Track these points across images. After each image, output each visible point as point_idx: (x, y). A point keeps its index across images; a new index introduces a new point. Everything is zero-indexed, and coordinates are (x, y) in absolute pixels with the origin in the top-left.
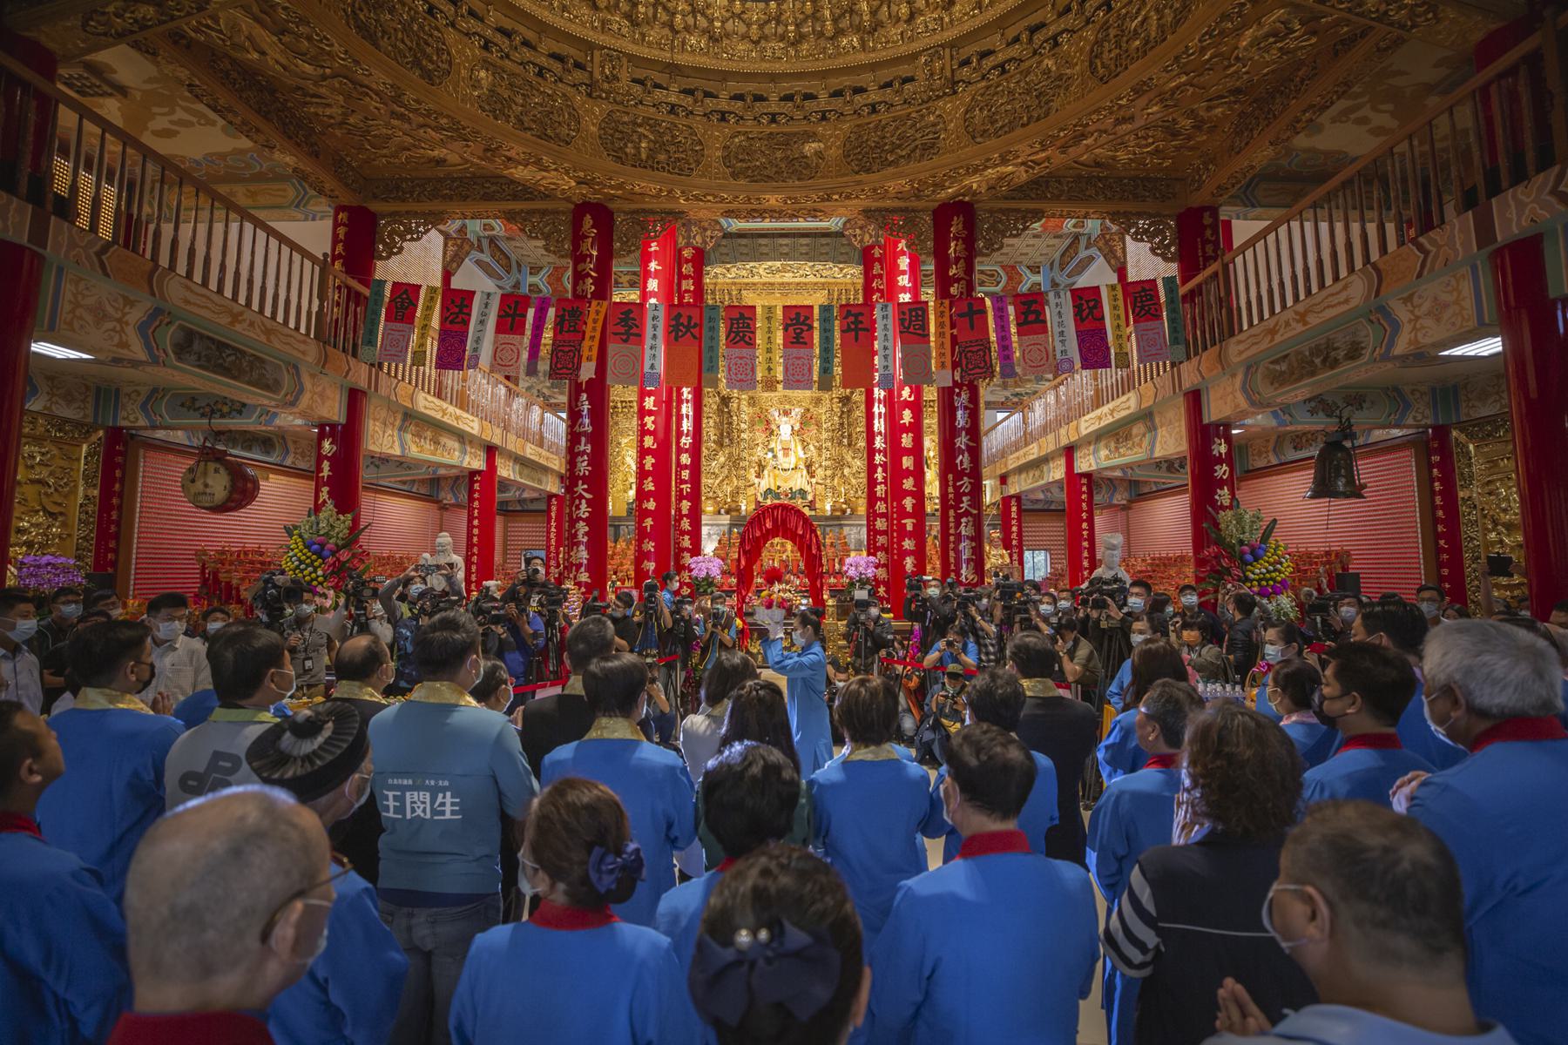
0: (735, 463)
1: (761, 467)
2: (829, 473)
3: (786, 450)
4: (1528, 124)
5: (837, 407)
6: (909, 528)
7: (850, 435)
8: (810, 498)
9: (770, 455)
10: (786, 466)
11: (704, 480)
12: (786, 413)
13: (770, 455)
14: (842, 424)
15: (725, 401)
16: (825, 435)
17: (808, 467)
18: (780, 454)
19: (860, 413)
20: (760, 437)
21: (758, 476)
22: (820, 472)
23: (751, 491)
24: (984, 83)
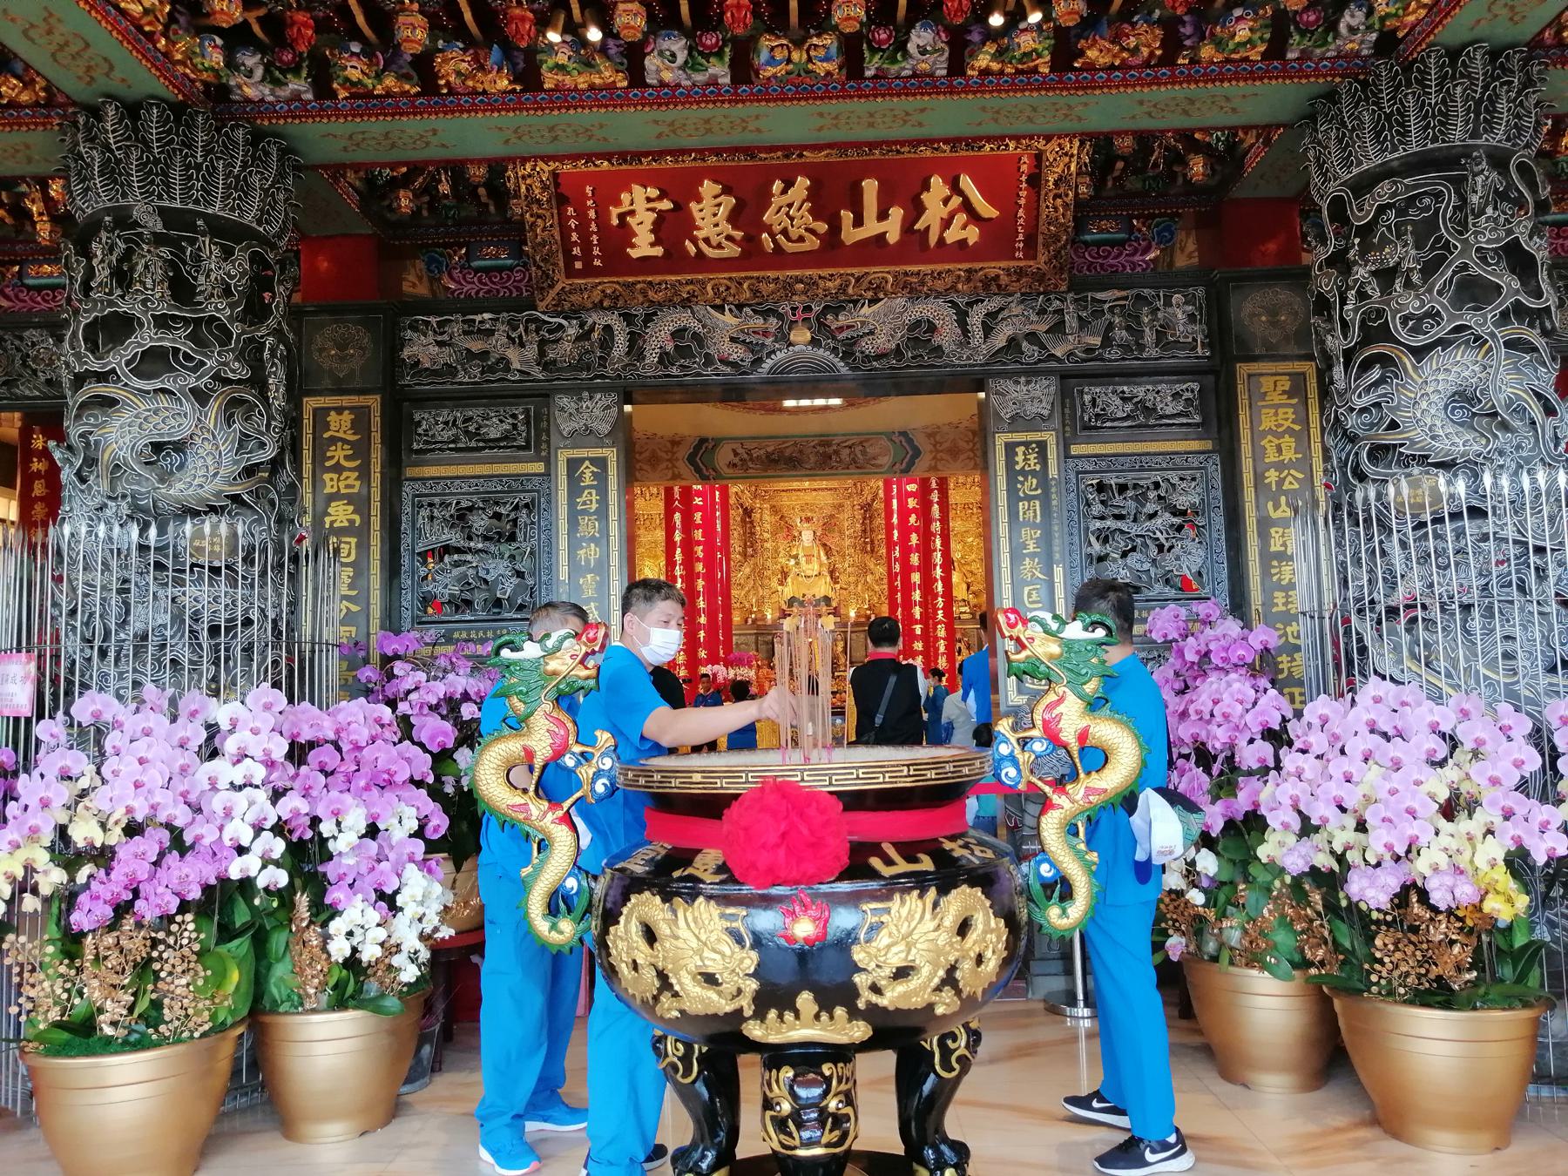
0: (759, 574)
1: (785, 575)
2: (852, 579)
3: (809, 557)
4: (1322, 548)
5: (859, 515)
6: (918, 632)
7: (872, 542)
8: (834, 604)
9: (792, 562)
10: (809, 573)
11: (734, 592)
12: (808, 520)
13: (792, 562)
14: (864, 531)
15: (748, 512)
16: (848, 542)
17: (832, 573)
18: (803, 560)
19: (880, 521)
20: (783, 545)
21: (781, 584)
22: (843, 578)
23: (775, 598)
24: (1476, 613)
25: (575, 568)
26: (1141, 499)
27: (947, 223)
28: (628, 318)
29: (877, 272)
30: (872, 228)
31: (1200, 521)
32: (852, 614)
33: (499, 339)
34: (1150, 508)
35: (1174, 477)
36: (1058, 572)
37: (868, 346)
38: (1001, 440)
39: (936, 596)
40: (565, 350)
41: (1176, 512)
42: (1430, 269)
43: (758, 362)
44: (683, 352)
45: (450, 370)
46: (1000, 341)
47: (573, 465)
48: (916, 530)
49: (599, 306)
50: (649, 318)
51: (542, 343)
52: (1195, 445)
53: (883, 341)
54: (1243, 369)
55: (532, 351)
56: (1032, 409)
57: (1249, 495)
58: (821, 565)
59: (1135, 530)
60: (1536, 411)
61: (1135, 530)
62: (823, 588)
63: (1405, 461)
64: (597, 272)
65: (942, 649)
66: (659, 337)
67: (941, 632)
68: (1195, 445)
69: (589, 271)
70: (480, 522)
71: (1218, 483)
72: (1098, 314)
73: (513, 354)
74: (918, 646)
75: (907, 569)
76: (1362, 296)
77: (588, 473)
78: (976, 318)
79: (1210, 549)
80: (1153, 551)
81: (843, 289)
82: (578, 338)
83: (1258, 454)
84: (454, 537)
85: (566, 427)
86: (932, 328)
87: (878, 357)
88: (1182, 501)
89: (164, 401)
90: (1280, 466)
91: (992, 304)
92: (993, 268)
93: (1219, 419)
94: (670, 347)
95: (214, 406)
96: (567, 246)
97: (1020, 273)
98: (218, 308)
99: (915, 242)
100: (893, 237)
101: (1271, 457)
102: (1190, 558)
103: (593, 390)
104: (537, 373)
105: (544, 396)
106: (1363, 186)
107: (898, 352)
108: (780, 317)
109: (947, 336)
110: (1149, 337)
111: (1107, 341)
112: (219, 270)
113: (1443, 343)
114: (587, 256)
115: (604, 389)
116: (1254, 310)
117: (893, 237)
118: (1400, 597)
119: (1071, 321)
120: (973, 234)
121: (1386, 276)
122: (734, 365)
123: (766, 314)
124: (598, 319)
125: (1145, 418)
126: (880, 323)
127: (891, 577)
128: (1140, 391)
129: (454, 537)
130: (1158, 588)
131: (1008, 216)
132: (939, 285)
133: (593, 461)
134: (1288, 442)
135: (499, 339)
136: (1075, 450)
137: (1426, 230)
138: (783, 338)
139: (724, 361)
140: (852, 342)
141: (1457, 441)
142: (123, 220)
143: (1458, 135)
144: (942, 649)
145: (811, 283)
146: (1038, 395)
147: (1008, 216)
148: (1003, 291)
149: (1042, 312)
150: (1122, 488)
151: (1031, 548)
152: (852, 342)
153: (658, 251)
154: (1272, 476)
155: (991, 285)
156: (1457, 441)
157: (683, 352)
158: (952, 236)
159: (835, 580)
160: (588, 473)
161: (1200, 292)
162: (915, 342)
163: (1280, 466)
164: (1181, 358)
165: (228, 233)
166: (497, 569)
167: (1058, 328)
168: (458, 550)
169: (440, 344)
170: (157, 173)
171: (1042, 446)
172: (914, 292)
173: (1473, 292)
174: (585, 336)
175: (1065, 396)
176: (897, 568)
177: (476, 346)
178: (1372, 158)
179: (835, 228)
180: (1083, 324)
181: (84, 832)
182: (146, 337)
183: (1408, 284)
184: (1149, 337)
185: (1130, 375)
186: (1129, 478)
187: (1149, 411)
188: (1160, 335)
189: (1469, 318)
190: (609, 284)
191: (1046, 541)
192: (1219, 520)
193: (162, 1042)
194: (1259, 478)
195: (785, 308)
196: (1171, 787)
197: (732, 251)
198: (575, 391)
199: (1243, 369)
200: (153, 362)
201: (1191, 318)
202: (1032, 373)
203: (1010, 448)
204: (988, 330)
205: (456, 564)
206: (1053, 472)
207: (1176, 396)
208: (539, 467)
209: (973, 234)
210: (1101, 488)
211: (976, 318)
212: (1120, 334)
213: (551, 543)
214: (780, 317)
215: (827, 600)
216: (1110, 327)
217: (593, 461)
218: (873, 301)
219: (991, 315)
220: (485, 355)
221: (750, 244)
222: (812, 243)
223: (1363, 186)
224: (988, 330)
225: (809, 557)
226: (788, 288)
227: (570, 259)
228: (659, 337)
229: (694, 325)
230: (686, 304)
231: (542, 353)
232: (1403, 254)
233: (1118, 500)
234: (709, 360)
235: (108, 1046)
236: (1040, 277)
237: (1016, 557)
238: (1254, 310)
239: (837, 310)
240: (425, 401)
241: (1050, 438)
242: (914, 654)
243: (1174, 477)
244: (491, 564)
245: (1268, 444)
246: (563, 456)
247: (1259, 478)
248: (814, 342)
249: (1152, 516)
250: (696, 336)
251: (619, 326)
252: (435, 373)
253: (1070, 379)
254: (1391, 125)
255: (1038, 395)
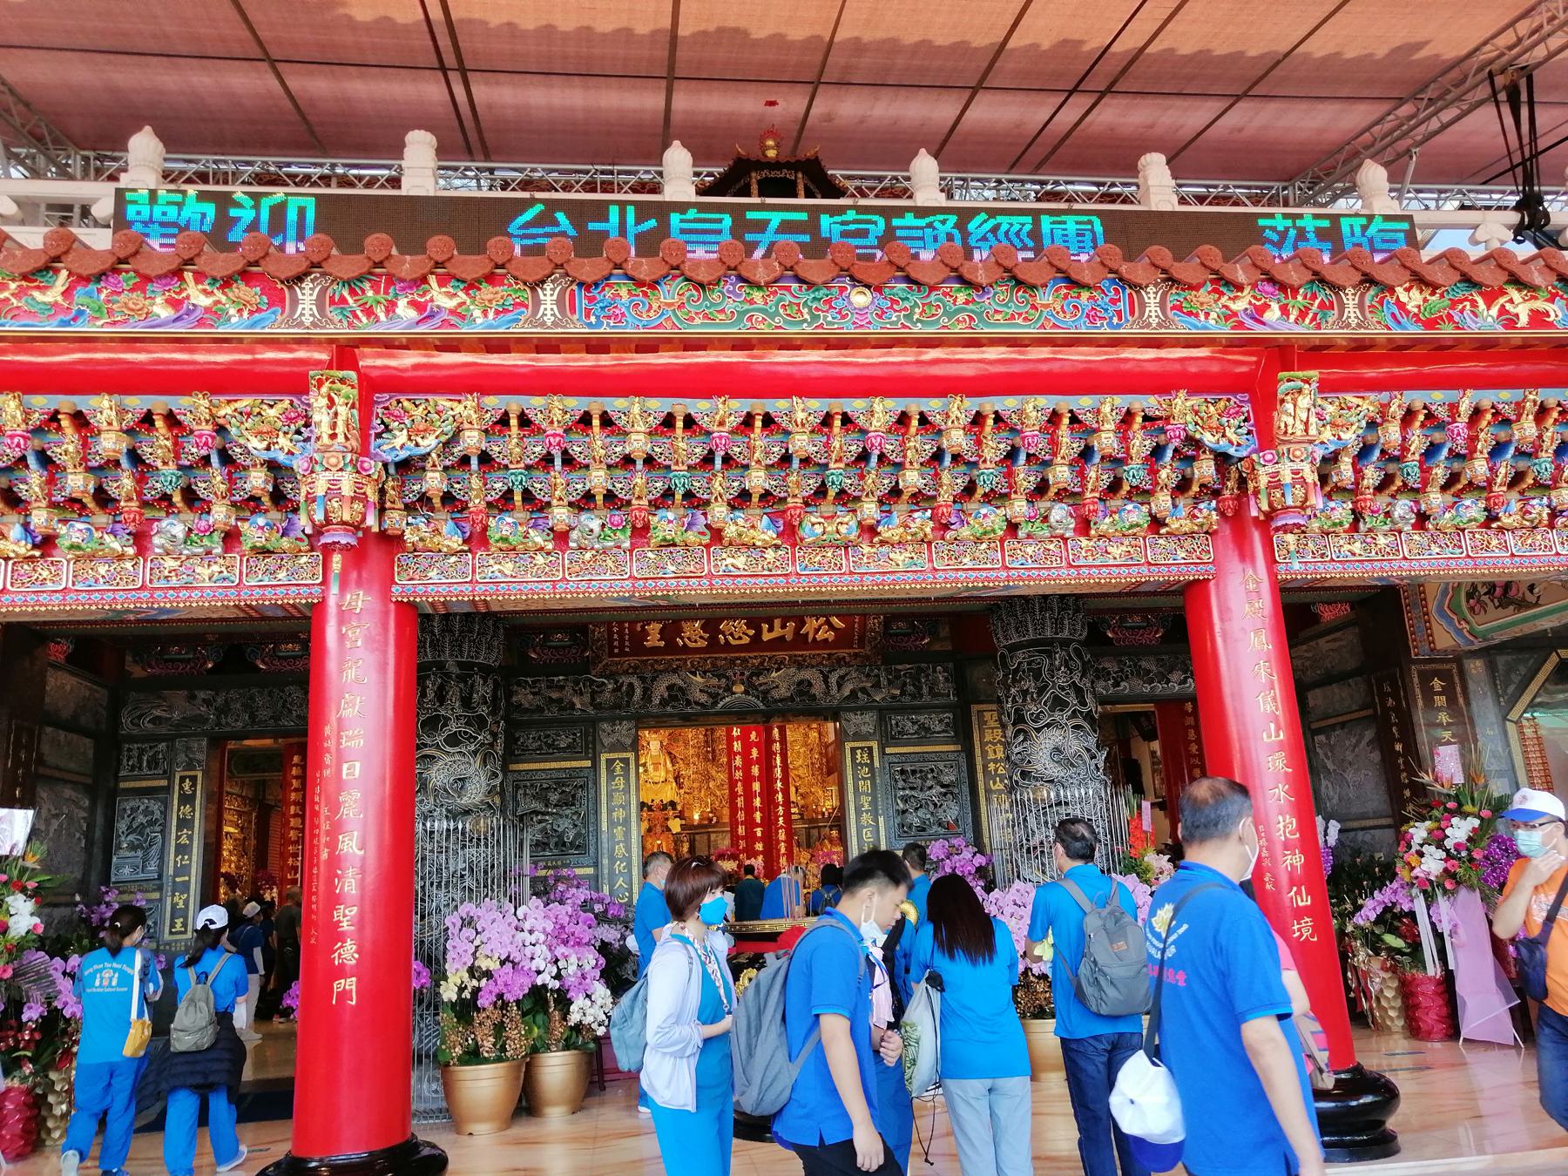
3: (656, 765)
16: (691, 751)
17: (677, 778)
18: (651, 768)
25: (612, 824)
26: (924, 779)
27: (817, 631)
28: (643, 680)
29: (780, 654)
30: (777, 632)
31: (956, 791)
32: (696, 817)
33: (568, 692)
34: (929, 783)
35: (941, 765)
36: (881, 819)
37: (775, 694)
38: (848, 746)
39: (777, 805)
40: (606, 697)
41: (943, 786)
42: (1041, 691)
43: (715, 703)
44: (673, 698)
45: (540, 709)
46: (847, 693)
47: (610, 762)
48: (757, 745)
49: (626, 673)
50: (654, 679)
51: (593, 693)
52: (952, 748)
53: (783, 692)
54: (975, 708)
55: (587, 698)
56: (864, 729)
57: (980, 776)
58: (667, 772)
59: (921, 796)
60: (1086, 757)
61: (921, 796)
62: (669, 793)
63: (1036, 779)
64: (627, 654)
65: (783, 851)
66: (660, 690)
67: (782, 836)
68: (952, 748)
69: (622, 654)
70: (554, 797)
71: (965, 768)
72: (898, 677)
73: (576, 700)
74: (759, 846)
75: (748, 780)
76: (1014, 701)
77: (618, 766)
78: (833, 679)
79: (962, 807)
80: (931, 807)
81: (762, 663)
82: (614, 690)
83: (984, 754)
84: (537, 805)
85: (606, 741)
86: (810, 684)
87: (781, 700)
88: (946, 779)
89: (457, 757)
90: (995, 761)
91: (842, 672)
92: (843, 653)
93: (963, 733)
94: (666, 695)
95: (479, 757)
96: (611, 640)
97: (856, 655)
98: (483, 710)
99: (800, 640)
100: (789, 637)
101: (991, 756)
102: (951, 812)
103: (622, 719)
104: (590, 710)
105: (594, 723)
106: (1013, 648)
107: (791, 699)
108: (728, 678)
109: (818, 689)
110: (925, 690)
111: (903, 693)
112: (483, 690)
113: (1048, 726)
114: (622, 646)
115: (628, 719)
116: (977, 674)
117: (789, 637)
118: (1035, 841)
119: (884, 682)
120: (831, 635)
121: (1025, 693)
122: (702, 705)
123: (719, 677)
124: (625, 680)
125: (925, 735)
126: (781, 681)
127: (732, 783)
128: (922, 718)
129: (537, 805)
130: (935, 828)
131: (850, 626)
132: (814, 662)
133: (622, 760)
134: (1000, 748)
135: (568, 692)
136: (888, 750)
137: (1037, 675)
138: (728, 690)
139: (697, 703)
140: (766, 692)
141: (1054, 771)
142: (441, 666)
143: (1049, 634)
144: (783, 851)
145: (745, 660)
146: (865, 722)
147: (850, 626)
148: (847, 665)
149: (868, 676)
150: (914, 772)
151: (866, 807)
152: (766, 692)
153: (662, 643)
154: (992, 766)
155: (841, 662)
156: (1054, 771)
157: (673, 698)
158: (820, 636)
159: (680, 786)
160: (618, 766)
161: (951, 665)
162: (801, 693)
163: (995, 761)
164: (942, 701)
165: (486, 671)
166: (564, 825)
167: (877, 685)
168: (543, 814)
169: (534, 694)
170: (457, 645)
171: (870, 749)
172: (800, 666)
173: (1059, 704)
174: (618, 689)
175: (882, 720)
176: (738, 775)
177: (555, 695)
178: (1015, 639)
179: (759, 632)
180: (890, 682)
181: (484, 964)
182: (453, 727)
183: (1033, 700)
184: (925, 690)
185: (917, 709)
186: (918, 766)
187: (928, 730)
188: (931, 689)
189: (1057, 716)
190: (634, 660)
191: (874, 803)
192: (966, 789)
193: (507, 1059)
194: (985, 767)
195: (730, 673)
196: (694, 735)
197: (702, 644)
198: (613, 720)
199: (975, 708)
200: (453, 740)
201: (946, 679)
202: (863, 709)
203: (853, 750)
204: (840, 686)
205: (540, 822)
206: (877, 764)
207: (941, 721)
208: (588, 763)
209: (831, 635)
210: (902, 772)
211: (833, 679)
212: (910, 688)
213: (597, 813)
214: (728, 678)
215: (673, 804)
216: (905, 684)
217: (622, 760)
218: (778, 670)
219: (842, 678)
220: (560, 700)
221: (713, 640)
222: (746, 640)
223: (1013, 648)
224: (840, 686)
225: (656, 765)
226: (732, 662)
227: (612, 648)
228: (660, 690)
229: (680, 682)
230: (675, 671)
231: (593, 699)
232: (1029, 684)
233: (912, 779)
234: (688, 703)
235: (486, 1061)
236: (867, 657)
237: (859, 813)
238: (977, 674)
239: (758, 675)
240: (529, 725)
241: (875, 745)
242: (754, 854)
243: (941, 765)
244: (561, 821)
245: (989, 748)
246: (604, 757)
247: (985, 767)
248: (746, 692)
249: (930, 788)
250: (681, 689)
251: (637, 683)
252: (533, 711)
253: (883, 713)
254: (1021, 627)
255: (865, 722)
